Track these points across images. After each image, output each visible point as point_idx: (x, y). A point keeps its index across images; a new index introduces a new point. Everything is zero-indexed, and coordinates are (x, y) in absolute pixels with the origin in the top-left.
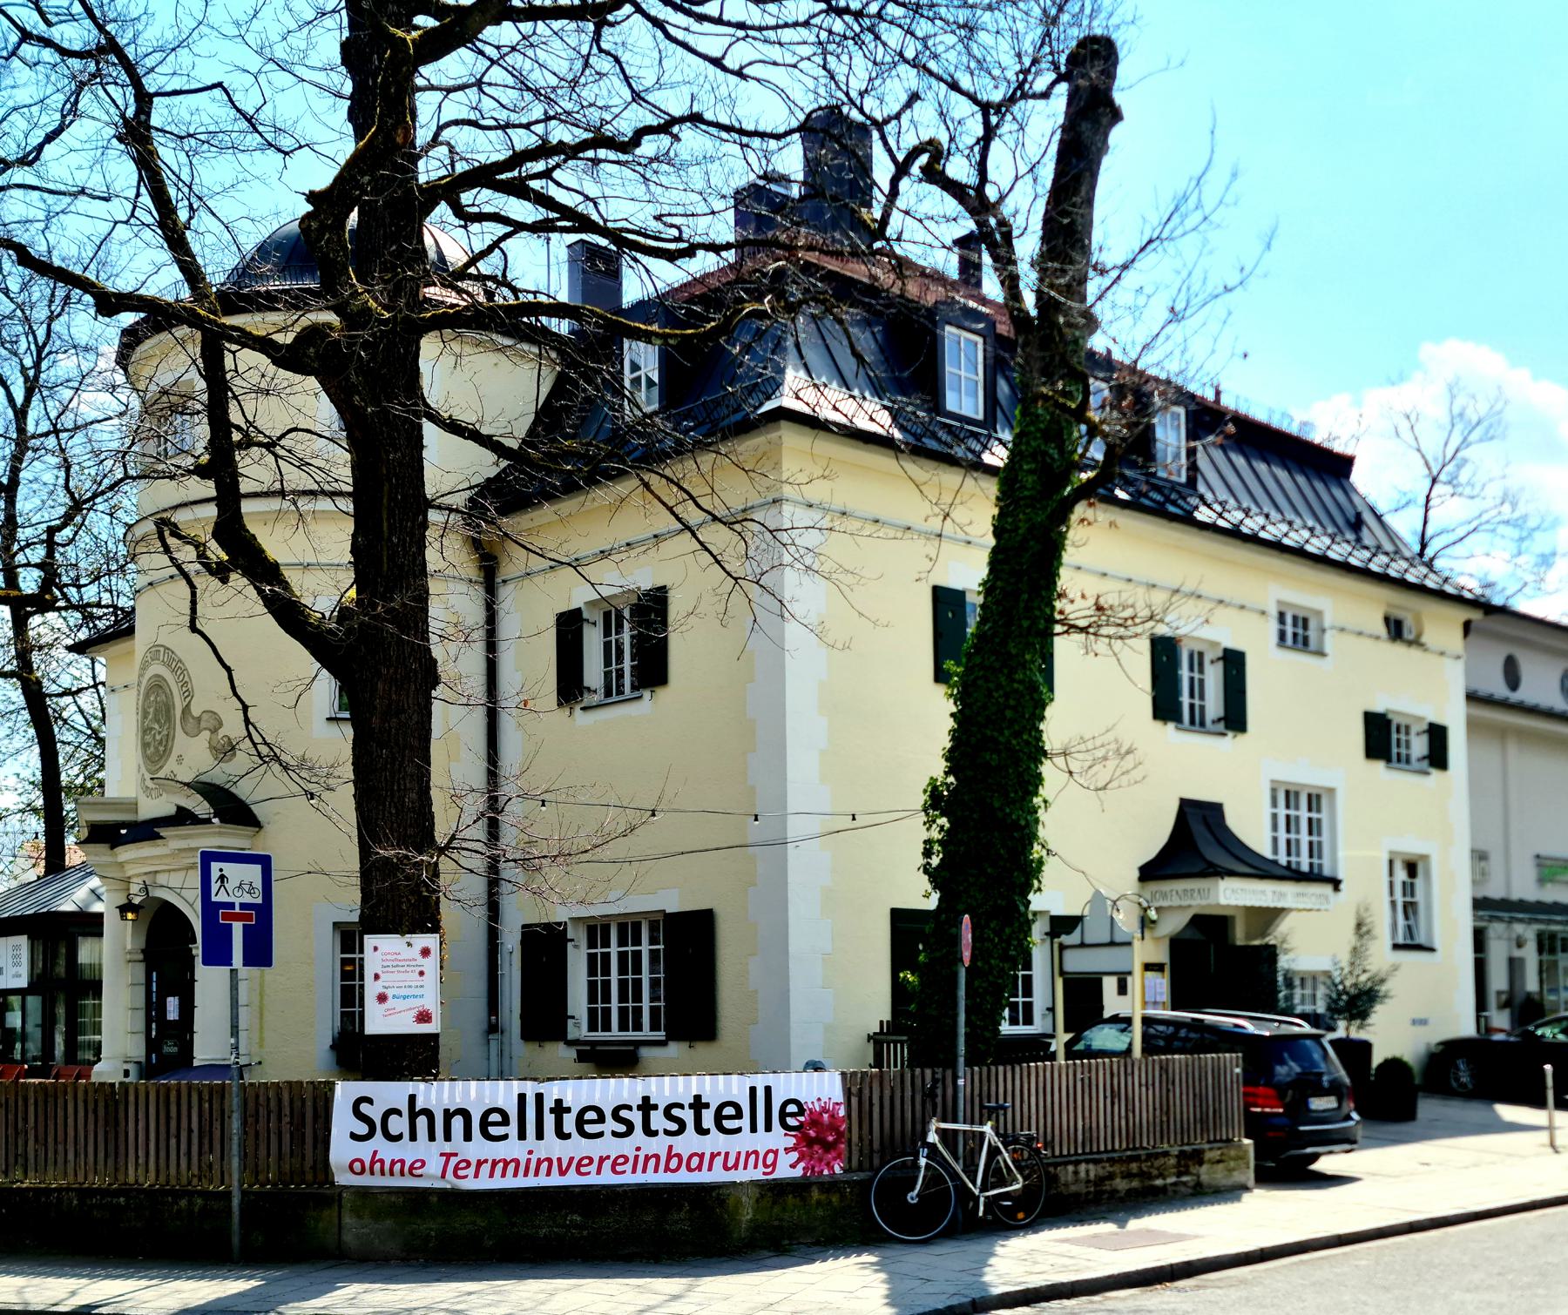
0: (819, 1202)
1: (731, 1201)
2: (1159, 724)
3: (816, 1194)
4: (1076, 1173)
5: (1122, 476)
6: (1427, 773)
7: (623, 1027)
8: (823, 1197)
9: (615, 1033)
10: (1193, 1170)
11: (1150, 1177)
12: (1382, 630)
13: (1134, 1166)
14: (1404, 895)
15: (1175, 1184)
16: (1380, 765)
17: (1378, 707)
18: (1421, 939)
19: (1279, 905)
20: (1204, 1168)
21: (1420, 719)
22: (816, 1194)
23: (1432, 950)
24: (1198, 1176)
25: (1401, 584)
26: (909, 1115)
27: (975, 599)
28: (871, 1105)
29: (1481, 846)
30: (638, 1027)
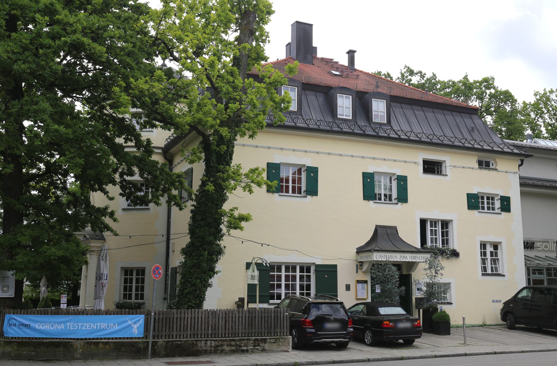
0: (102, 348)
1: (75, 346)
2: (366, 202)
3: (101, 345)
4: (211, 343)
5: (31, 186)
6: (501, 214)
7: (137, 298)
8: (103, 346)
9: (133, 300)
10: (262, 345)
11: (240, 346)
12: (477, 166)
13: (233, 343)
14: (491, 256)
15: (252, 349)
16: (475, 212)
17: (474, 191)
18: (500, 272)
19: (414, 261)
20: (267, 344)
21: (498, 195)
22: (101, 345)
23: (504, 276)
24: (264, 347)
25: (483, 150)
26: (182, 325)
27: (122, 192)
28: (271, 325)
29: (532, 237)
30: (130, 298)
